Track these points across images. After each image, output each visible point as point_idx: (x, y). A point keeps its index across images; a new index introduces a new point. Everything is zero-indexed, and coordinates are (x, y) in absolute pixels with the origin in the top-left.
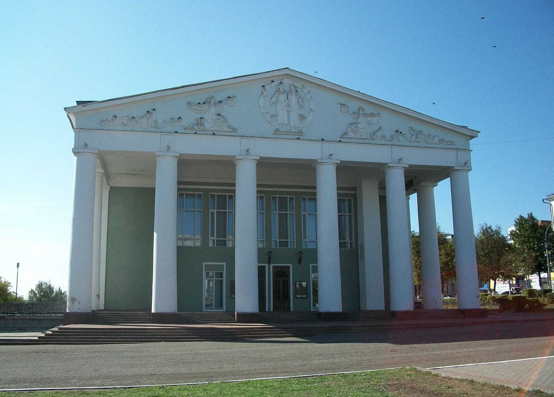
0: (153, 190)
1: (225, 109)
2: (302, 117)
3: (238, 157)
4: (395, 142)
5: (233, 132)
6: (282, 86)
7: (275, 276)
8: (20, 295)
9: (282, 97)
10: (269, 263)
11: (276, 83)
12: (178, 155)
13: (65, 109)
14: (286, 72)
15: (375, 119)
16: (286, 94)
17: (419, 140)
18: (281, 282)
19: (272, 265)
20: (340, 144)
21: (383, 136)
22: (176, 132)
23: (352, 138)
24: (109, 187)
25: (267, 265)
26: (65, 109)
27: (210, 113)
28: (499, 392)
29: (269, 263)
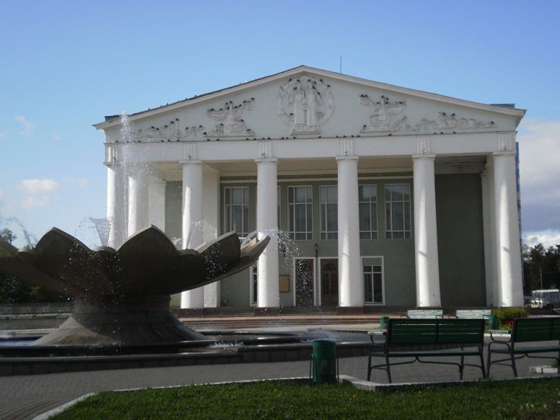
0: (182, 182)
1: (245, 114)
2: (319, 115)
3: (494, 153)
4: (422, 131)
5: (250, 137)
6: (299, 85)
7: (323, 269)
8: (38, 234)
9: (298, 97)
10: (317, 256)
11: (294, 81)
12: (434, 156)
13: (525, 111)
14: (301, 70)
15: (400, 108)
16: (303, 92)
17: (450, 126)
18: (330, 275)
19: (319, 258)
20: (218, 142)
21: (408, 126)
22: (454, 133)
23: (372, 132)
24: (165, 182)
25: (314, 258)
26: (525, 111)
27: (229, 120)
28: (246, 412)
29: (317, 256)
